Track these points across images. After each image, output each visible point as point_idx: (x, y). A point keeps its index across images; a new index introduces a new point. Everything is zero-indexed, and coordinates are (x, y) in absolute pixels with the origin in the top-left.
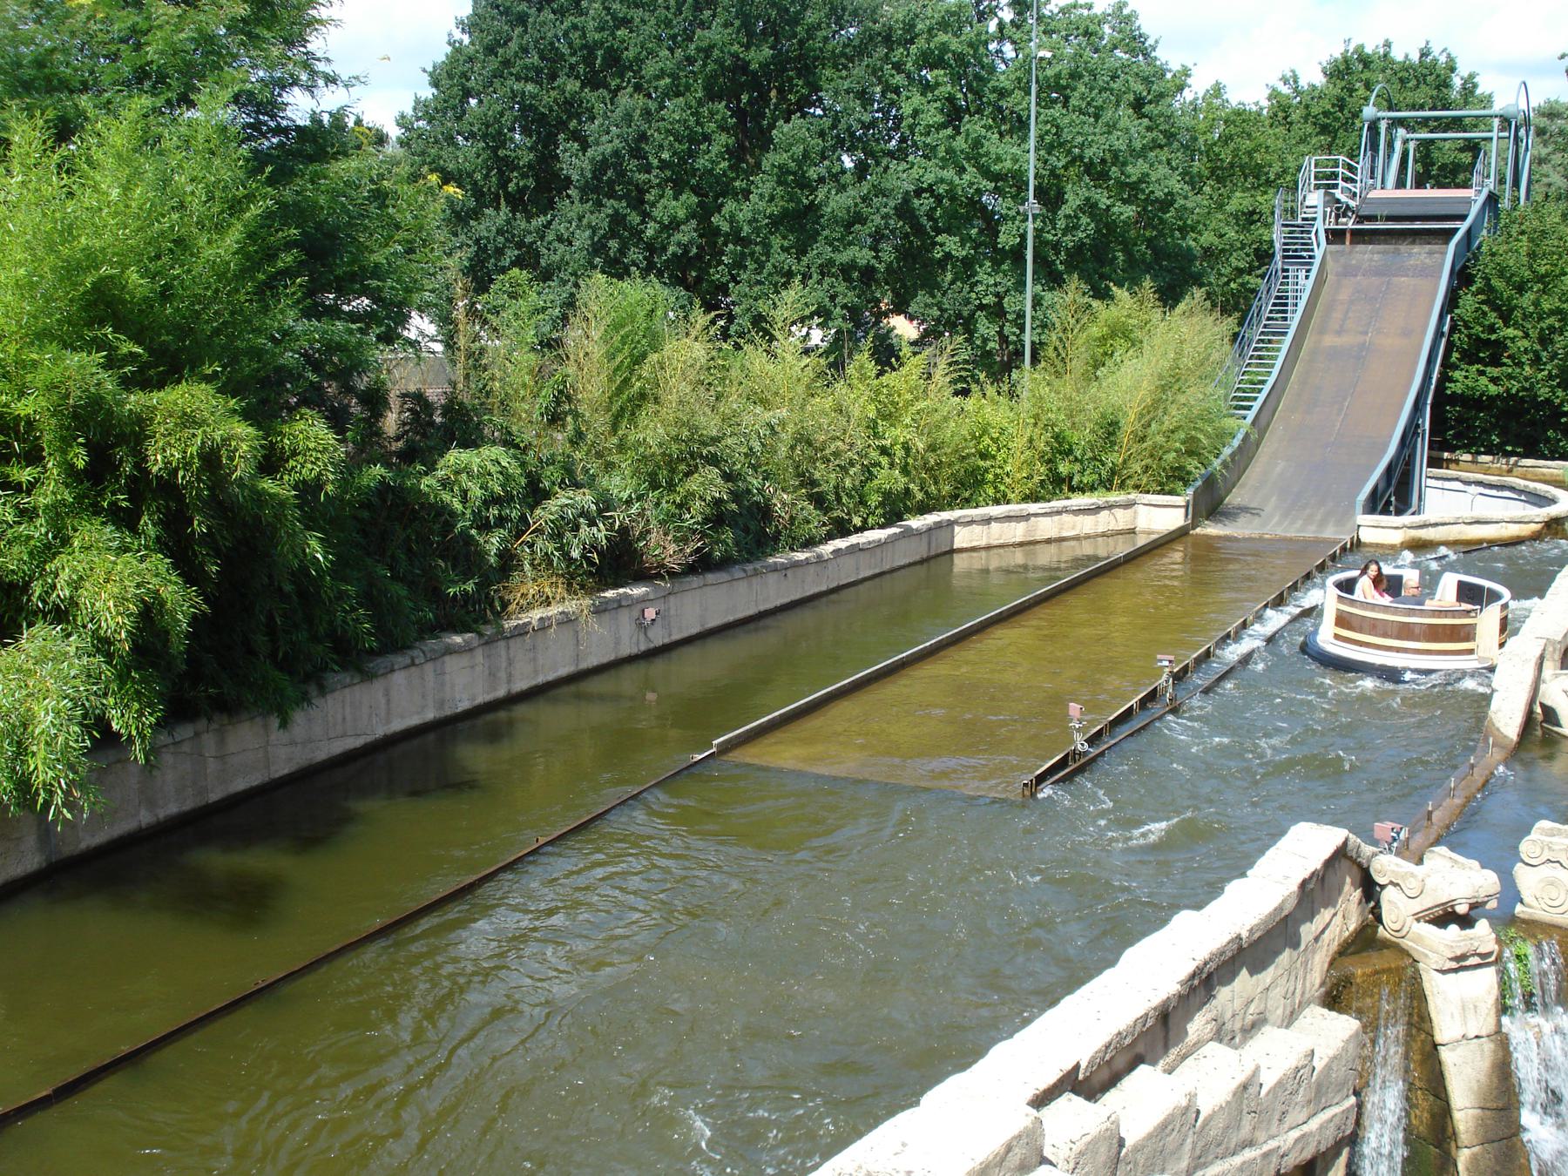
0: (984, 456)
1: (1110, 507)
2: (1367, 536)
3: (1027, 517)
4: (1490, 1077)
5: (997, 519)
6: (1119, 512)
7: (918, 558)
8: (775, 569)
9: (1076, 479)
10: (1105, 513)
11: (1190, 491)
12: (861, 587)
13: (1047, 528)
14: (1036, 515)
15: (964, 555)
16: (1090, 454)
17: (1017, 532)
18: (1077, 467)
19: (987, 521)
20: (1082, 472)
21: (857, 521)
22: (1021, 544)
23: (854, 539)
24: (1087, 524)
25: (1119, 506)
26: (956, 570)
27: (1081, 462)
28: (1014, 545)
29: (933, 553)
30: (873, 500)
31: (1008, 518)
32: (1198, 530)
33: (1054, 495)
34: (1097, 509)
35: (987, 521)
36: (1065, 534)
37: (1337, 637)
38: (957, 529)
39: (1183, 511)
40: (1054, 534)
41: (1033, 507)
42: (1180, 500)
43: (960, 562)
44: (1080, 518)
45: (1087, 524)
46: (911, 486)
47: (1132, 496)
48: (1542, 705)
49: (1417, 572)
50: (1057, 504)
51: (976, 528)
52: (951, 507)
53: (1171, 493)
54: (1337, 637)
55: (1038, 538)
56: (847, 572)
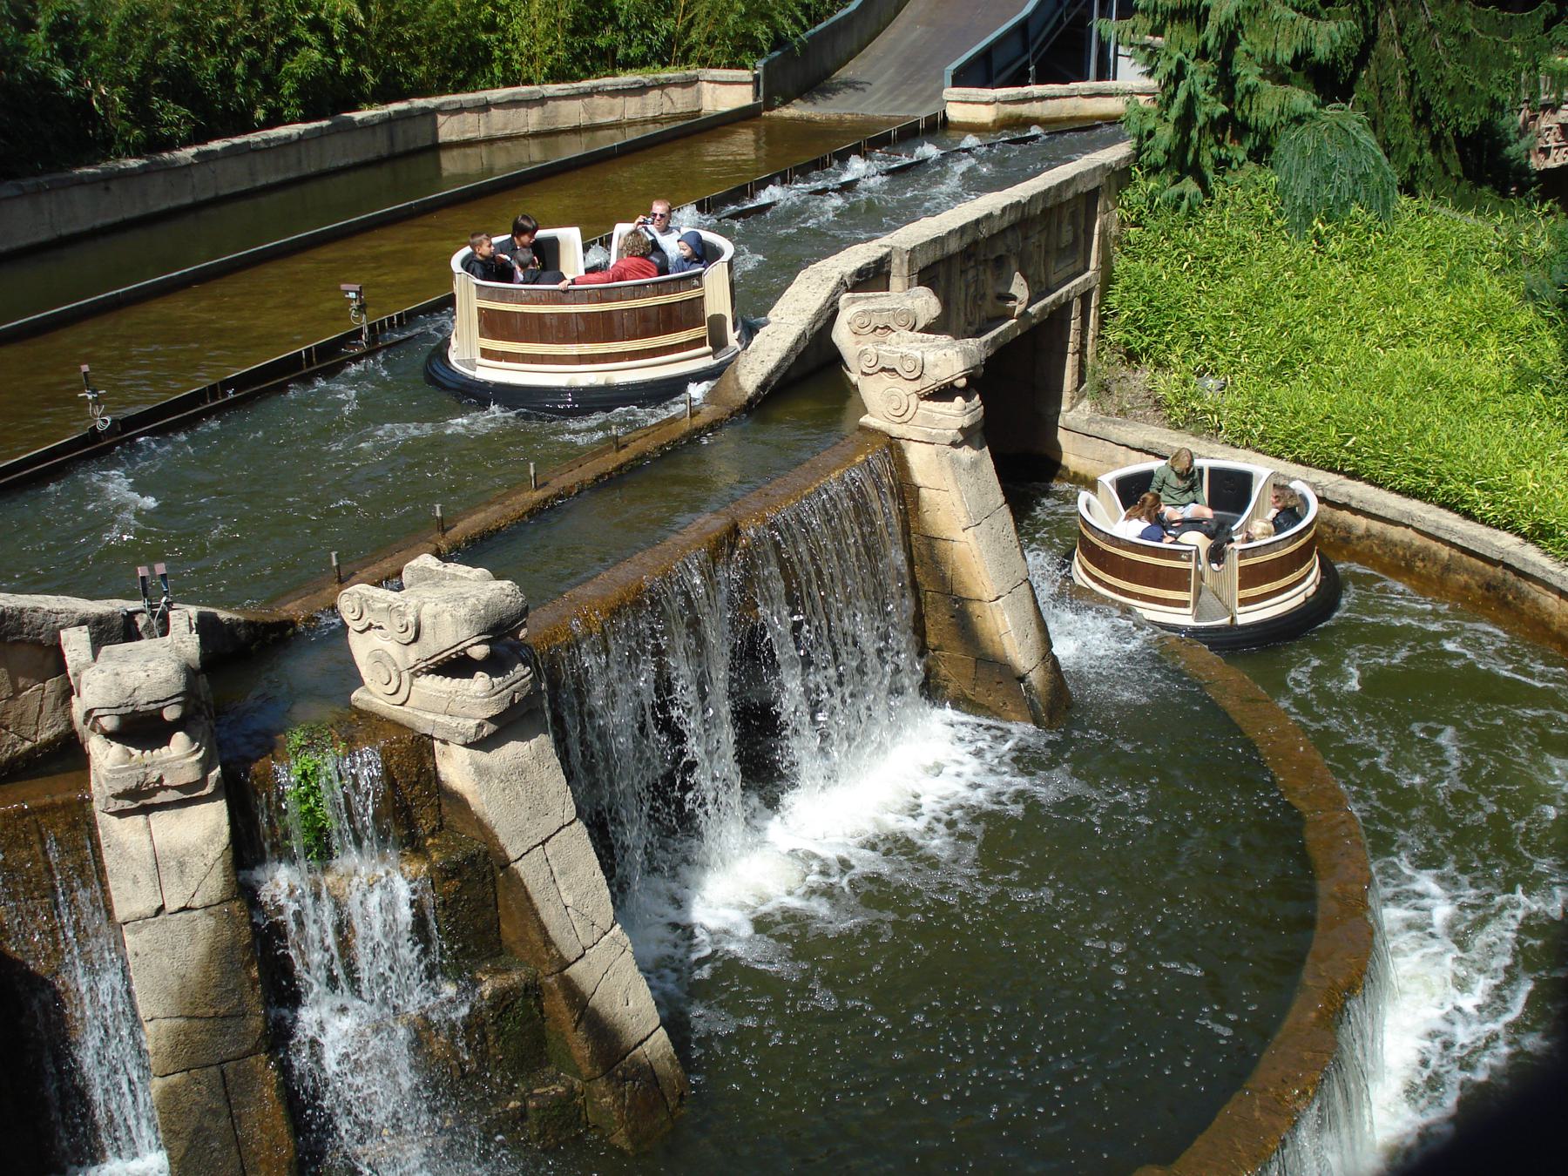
0: (491, 27)
1: (662, 86)
2: (956, 113)
3: (542, 101)
4: (999, 653)
5: (498, 105)
6: (676, 93)
7: (371, 156)
8: (81, 182)
9: (620, 53)
10: (656, 93)
11: (760, 64)
12: (264, 201)
13: (572, 113)
14: (554, 98)
15: (455, 152)
16: (635, 22)
17: (532, 119)
18: (622, 37)
19: (485, 107)
20: (629, 44)
21: (260, 114)
22: (536, 135)
23: (252, 138)
24: (631, 108)
25: (676, 84)
26: (445, 174)
27: (626, 30)
28: (527, 136)
29: (400, 148)
30: (288, 87)
31: (514, 103)
32: (775, 113)
33: (589, 73)
34: (642, 89)
35: (485, 107)
36: (599, 120)
37: (486, 353)
38: (441, 119)
39: (750, 87)
40: (583, 120)
41: (551, 89)
42: (746, 75)
43: (450, 164)
44: (620, 100)
45: (631, 108)
46: (362, 68)
47: (693, 72)
48: (1141, 537)
49: (1189, 178)
50: (586, 84)
51: (471, 118)
52: (442, 91)
53: (744, 67)
54: (486, 353)
55: (561, 126)
56: (235, 179)
